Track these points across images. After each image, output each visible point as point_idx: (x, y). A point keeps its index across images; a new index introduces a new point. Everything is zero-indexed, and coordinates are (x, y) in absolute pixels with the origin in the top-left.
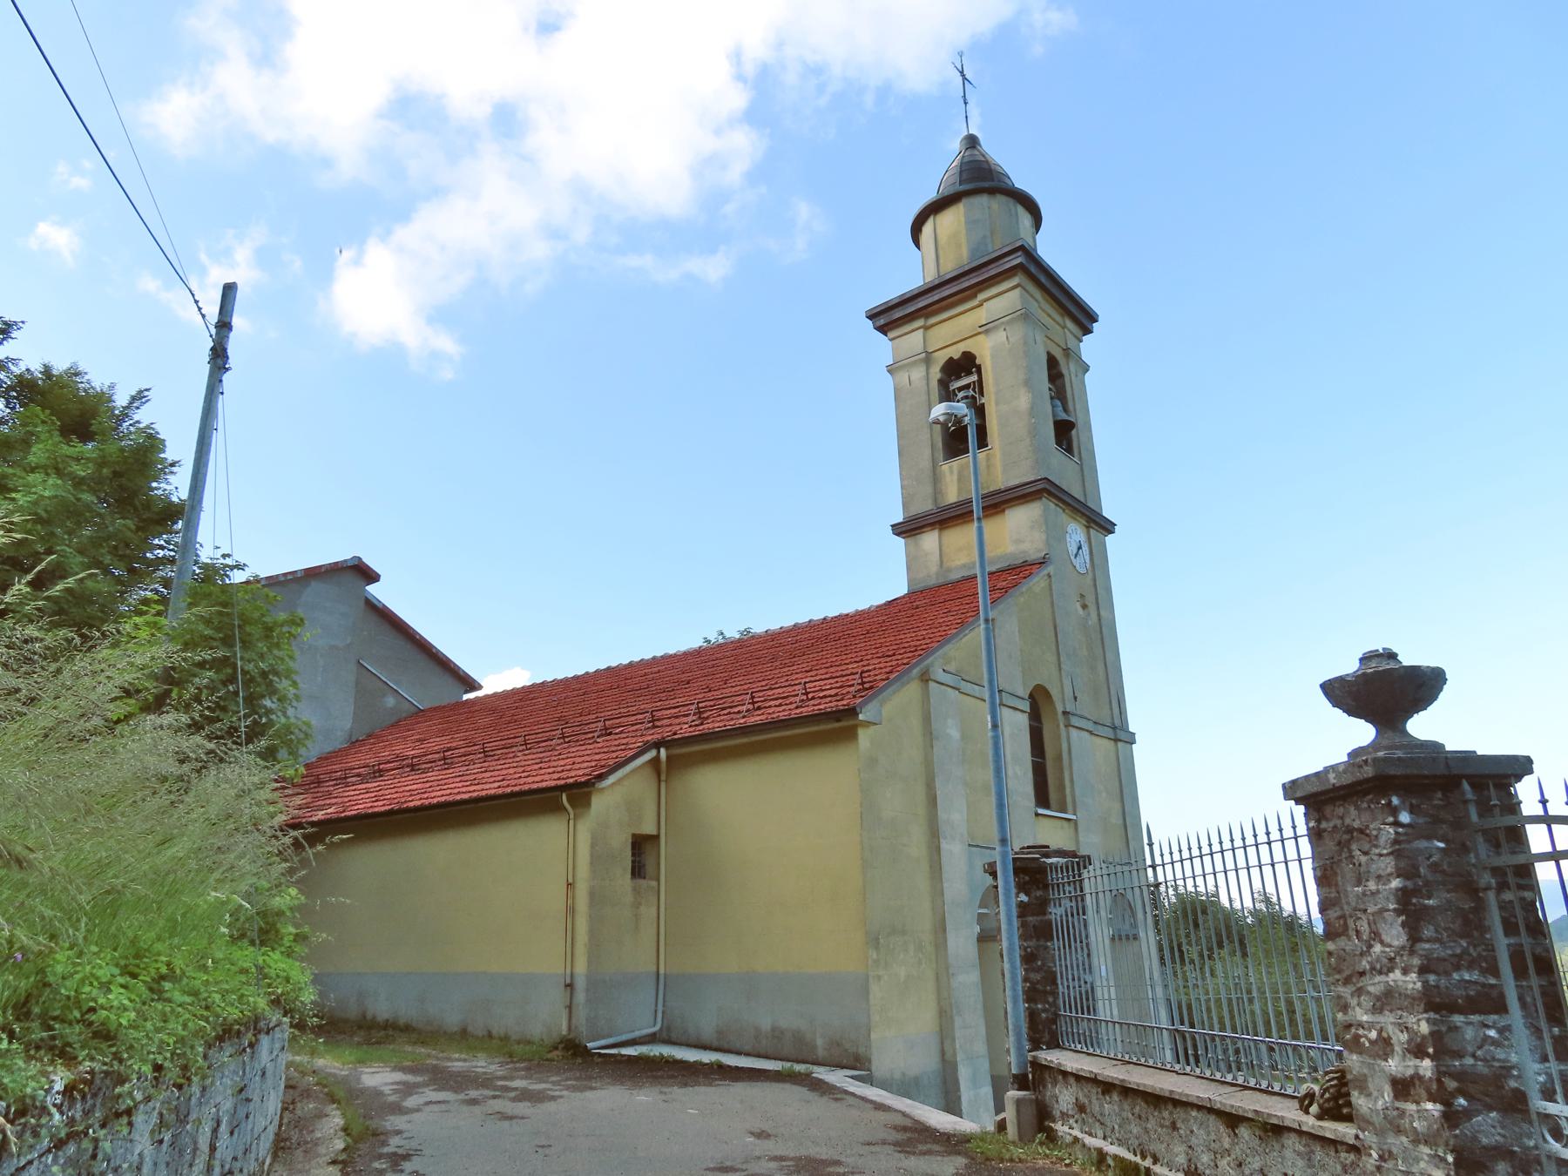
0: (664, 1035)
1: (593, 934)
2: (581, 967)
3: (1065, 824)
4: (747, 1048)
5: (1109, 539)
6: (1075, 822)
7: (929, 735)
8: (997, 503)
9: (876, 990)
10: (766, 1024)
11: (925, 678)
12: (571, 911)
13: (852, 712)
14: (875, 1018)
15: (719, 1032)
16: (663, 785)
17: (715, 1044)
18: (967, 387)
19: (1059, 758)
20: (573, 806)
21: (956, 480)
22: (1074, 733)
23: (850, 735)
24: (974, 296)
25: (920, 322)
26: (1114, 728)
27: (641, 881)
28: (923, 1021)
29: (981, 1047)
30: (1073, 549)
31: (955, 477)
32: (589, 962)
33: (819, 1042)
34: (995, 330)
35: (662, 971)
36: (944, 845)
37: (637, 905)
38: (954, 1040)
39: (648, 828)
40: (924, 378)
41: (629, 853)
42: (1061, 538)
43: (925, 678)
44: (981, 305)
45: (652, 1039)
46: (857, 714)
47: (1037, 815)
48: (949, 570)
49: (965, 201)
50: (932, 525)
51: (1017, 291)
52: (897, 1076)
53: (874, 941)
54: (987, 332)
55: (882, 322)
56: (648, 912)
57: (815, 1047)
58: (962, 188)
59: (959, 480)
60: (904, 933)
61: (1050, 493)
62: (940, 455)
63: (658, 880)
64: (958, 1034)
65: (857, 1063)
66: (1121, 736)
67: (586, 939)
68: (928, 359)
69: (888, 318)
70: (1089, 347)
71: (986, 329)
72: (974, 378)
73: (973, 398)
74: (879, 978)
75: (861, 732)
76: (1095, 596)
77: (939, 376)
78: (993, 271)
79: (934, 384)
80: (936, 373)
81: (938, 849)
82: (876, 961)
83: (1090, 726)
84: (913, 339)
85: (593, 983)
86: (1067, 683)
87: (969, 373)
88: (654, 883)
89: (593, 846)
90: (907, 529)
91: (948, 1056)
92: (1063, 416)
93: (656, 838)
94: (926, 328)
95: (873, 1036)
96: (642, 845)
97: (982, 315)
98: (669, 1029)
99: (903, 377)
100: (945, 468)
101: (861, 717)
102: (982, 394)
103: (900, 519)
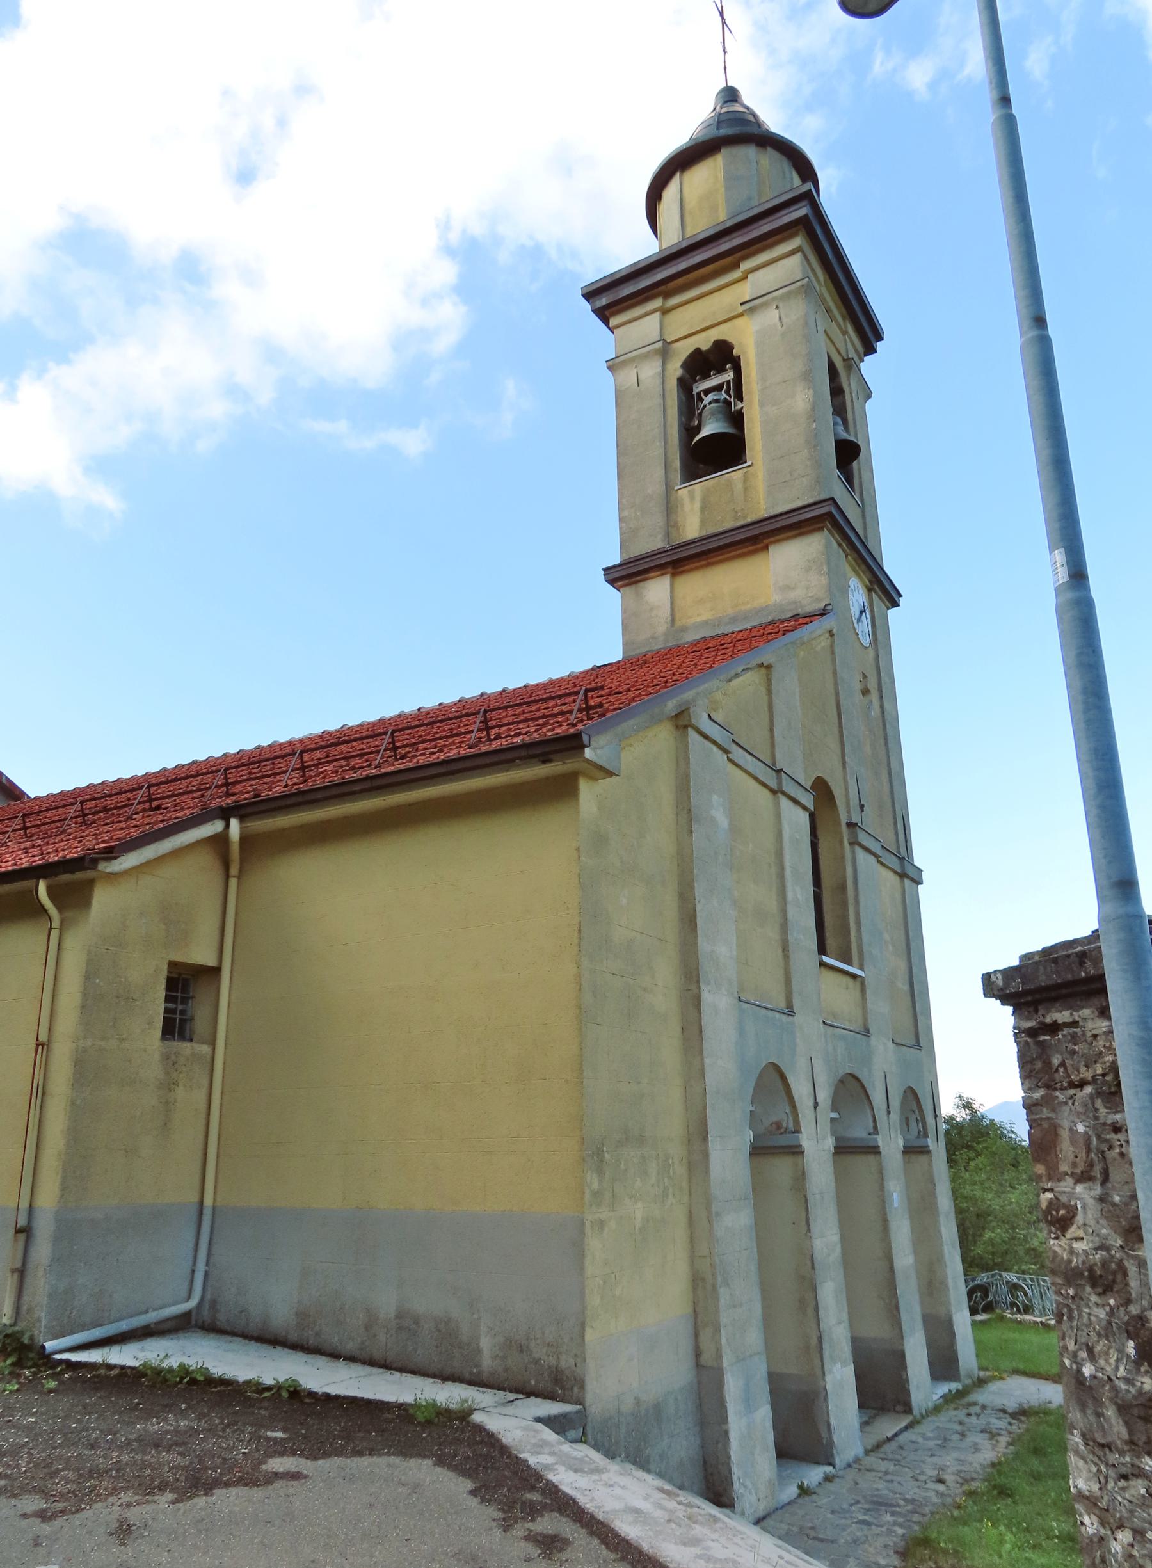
0: (206, 1314)
1: (75, 1135)
2: (48, 1198)
3: (846, 980)
4: (350, 1347)
5: (892, 613)
6: (863, 985)
7: (687, 813)
8: (753, 539)
9: (594, 1245)
10: (386, 1303)
11: (682, 721)
12: (39, 1093)
13: (573, 744)
14: (594, 1300)
15: (302, 1316)
16: (233, 882)
17: (293, 1336)
18: (718, 388)
19: (843, 888)
20: (60, 909)
21: (699, 508)
22: (861, 854)
23: (563, 790)
24: (736, 266)
25: (658, 303)
26: (902, 859)
27: (186, 1048)
28: (662, 1300)
29: (754, 1338)
30: (855, 610)
31: (697, 505)
32: (64, 1188)
33: (486, 1344)
34: (761, 315)
35: (208, 1201)
36: (707, 996)
37: (169, 1085)
38: (717, 1330)
39: (203, 956)
40: (658, 380)
41: (162, 994)
42: (844, 590)
43: (682, 721)
44: (744, 278)
45: (181, 1325)
46: (582, 747)
47: (822, 964)
48: (684, 629)
49: (725, 151)
50: (661, 568)
51: (798, 256)
52: (628, 1406)
53: (594, 1155)
54: (752, 310)
55: (603, 301)
56: (189, 1098)
57: (479, 1351)
58: (723, 132)
59: (703, 509)
60: (641, 1140)
61: (836, 526)
62: (677, 476)
63: (213, 1043)
64: (724, 1320)
65: (551, 1383)
66: (909, 875)
67: (61, 1144)
68: (665, 351)
69: (612, 297)
70: (869, 366)
71: (751, 307)
72: (729, 376)
73: (727, 403)
74: (601, 1224)
75: (584, 785)
76: (878, 685)
77: (679, 372)
78: (766, 227)
79: (673, 385)
80: (675, 369)
81: (697, 1002)
82: (596, 1194)
83: (879, 851)
84: (644, 326)
85: (68, 1228)
86: (852, 783)
87: (721, 370)
88: (205, 1049)
89: (88, 977)
90: (626, 575)
91: (707, 1358)
92: (844, 435)
93: (216, 971)
94: (665, 312)
95: (589, 1336)
96: (185, 984)
97: (746, 290)
98: (214, 1304)
99: (629, 376)
100: (684, 493)
101: (588, 753)
102: (739, 397)
103: (616, 560)
